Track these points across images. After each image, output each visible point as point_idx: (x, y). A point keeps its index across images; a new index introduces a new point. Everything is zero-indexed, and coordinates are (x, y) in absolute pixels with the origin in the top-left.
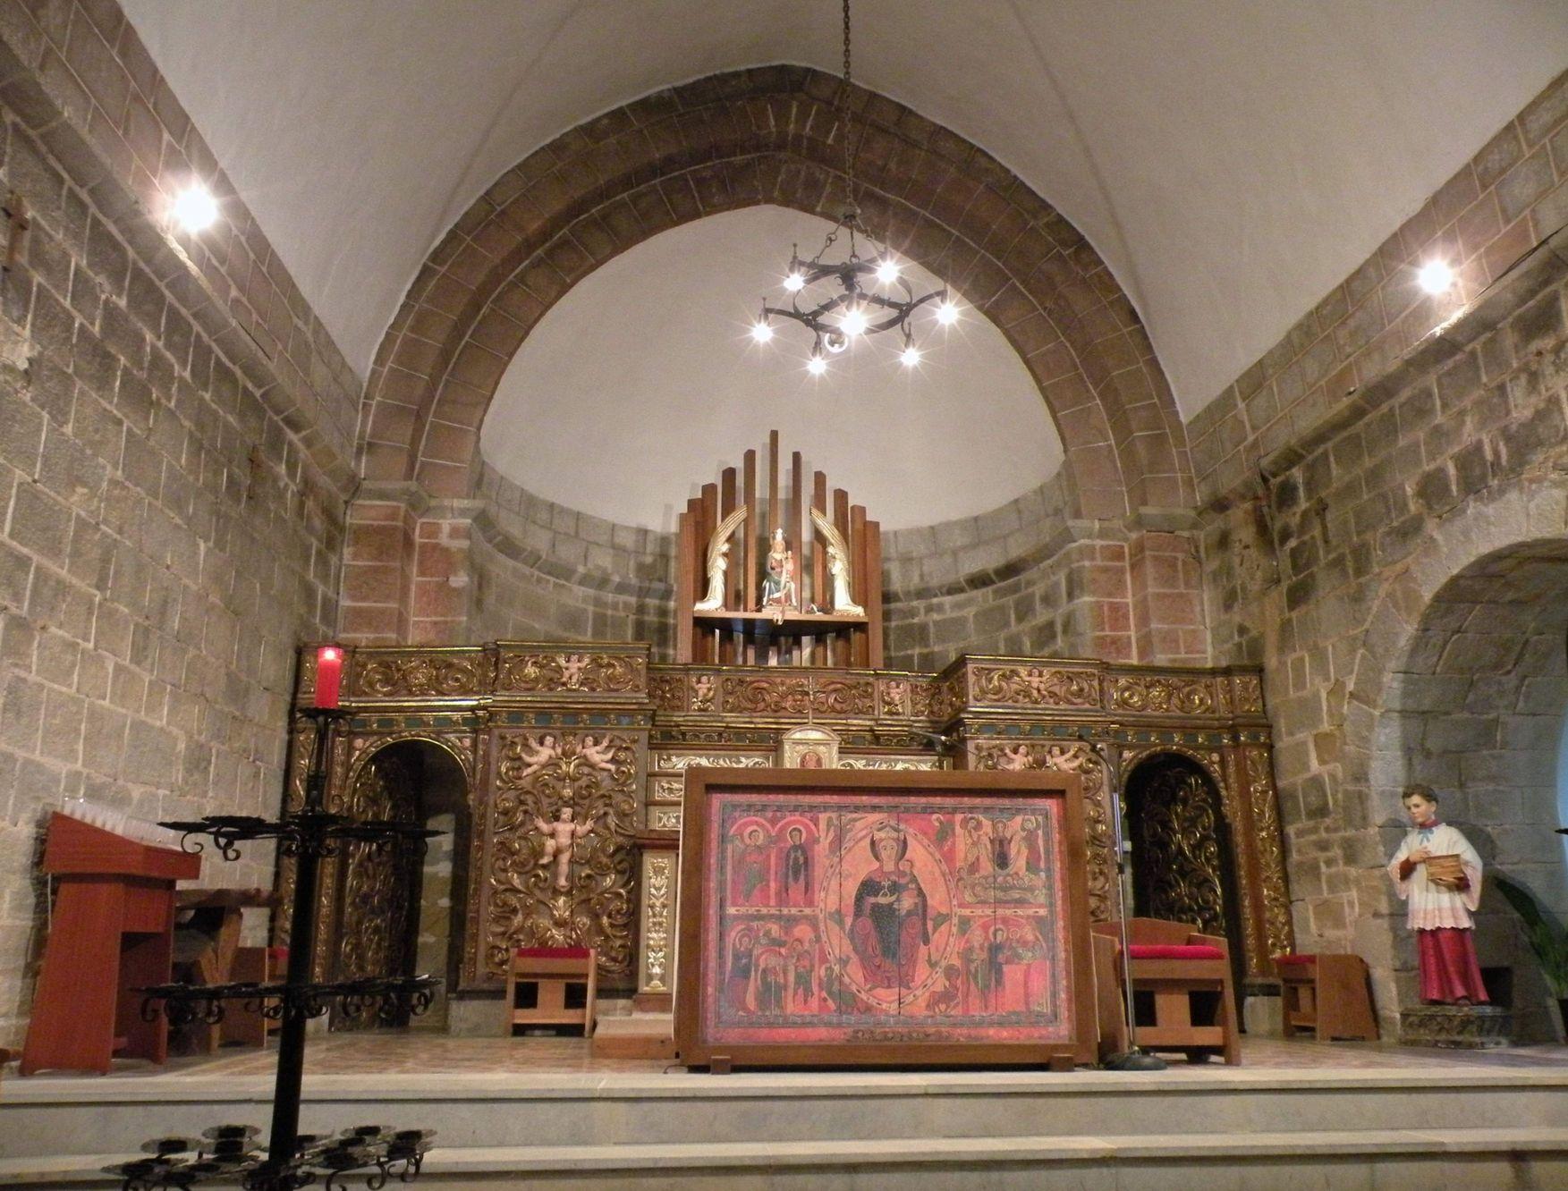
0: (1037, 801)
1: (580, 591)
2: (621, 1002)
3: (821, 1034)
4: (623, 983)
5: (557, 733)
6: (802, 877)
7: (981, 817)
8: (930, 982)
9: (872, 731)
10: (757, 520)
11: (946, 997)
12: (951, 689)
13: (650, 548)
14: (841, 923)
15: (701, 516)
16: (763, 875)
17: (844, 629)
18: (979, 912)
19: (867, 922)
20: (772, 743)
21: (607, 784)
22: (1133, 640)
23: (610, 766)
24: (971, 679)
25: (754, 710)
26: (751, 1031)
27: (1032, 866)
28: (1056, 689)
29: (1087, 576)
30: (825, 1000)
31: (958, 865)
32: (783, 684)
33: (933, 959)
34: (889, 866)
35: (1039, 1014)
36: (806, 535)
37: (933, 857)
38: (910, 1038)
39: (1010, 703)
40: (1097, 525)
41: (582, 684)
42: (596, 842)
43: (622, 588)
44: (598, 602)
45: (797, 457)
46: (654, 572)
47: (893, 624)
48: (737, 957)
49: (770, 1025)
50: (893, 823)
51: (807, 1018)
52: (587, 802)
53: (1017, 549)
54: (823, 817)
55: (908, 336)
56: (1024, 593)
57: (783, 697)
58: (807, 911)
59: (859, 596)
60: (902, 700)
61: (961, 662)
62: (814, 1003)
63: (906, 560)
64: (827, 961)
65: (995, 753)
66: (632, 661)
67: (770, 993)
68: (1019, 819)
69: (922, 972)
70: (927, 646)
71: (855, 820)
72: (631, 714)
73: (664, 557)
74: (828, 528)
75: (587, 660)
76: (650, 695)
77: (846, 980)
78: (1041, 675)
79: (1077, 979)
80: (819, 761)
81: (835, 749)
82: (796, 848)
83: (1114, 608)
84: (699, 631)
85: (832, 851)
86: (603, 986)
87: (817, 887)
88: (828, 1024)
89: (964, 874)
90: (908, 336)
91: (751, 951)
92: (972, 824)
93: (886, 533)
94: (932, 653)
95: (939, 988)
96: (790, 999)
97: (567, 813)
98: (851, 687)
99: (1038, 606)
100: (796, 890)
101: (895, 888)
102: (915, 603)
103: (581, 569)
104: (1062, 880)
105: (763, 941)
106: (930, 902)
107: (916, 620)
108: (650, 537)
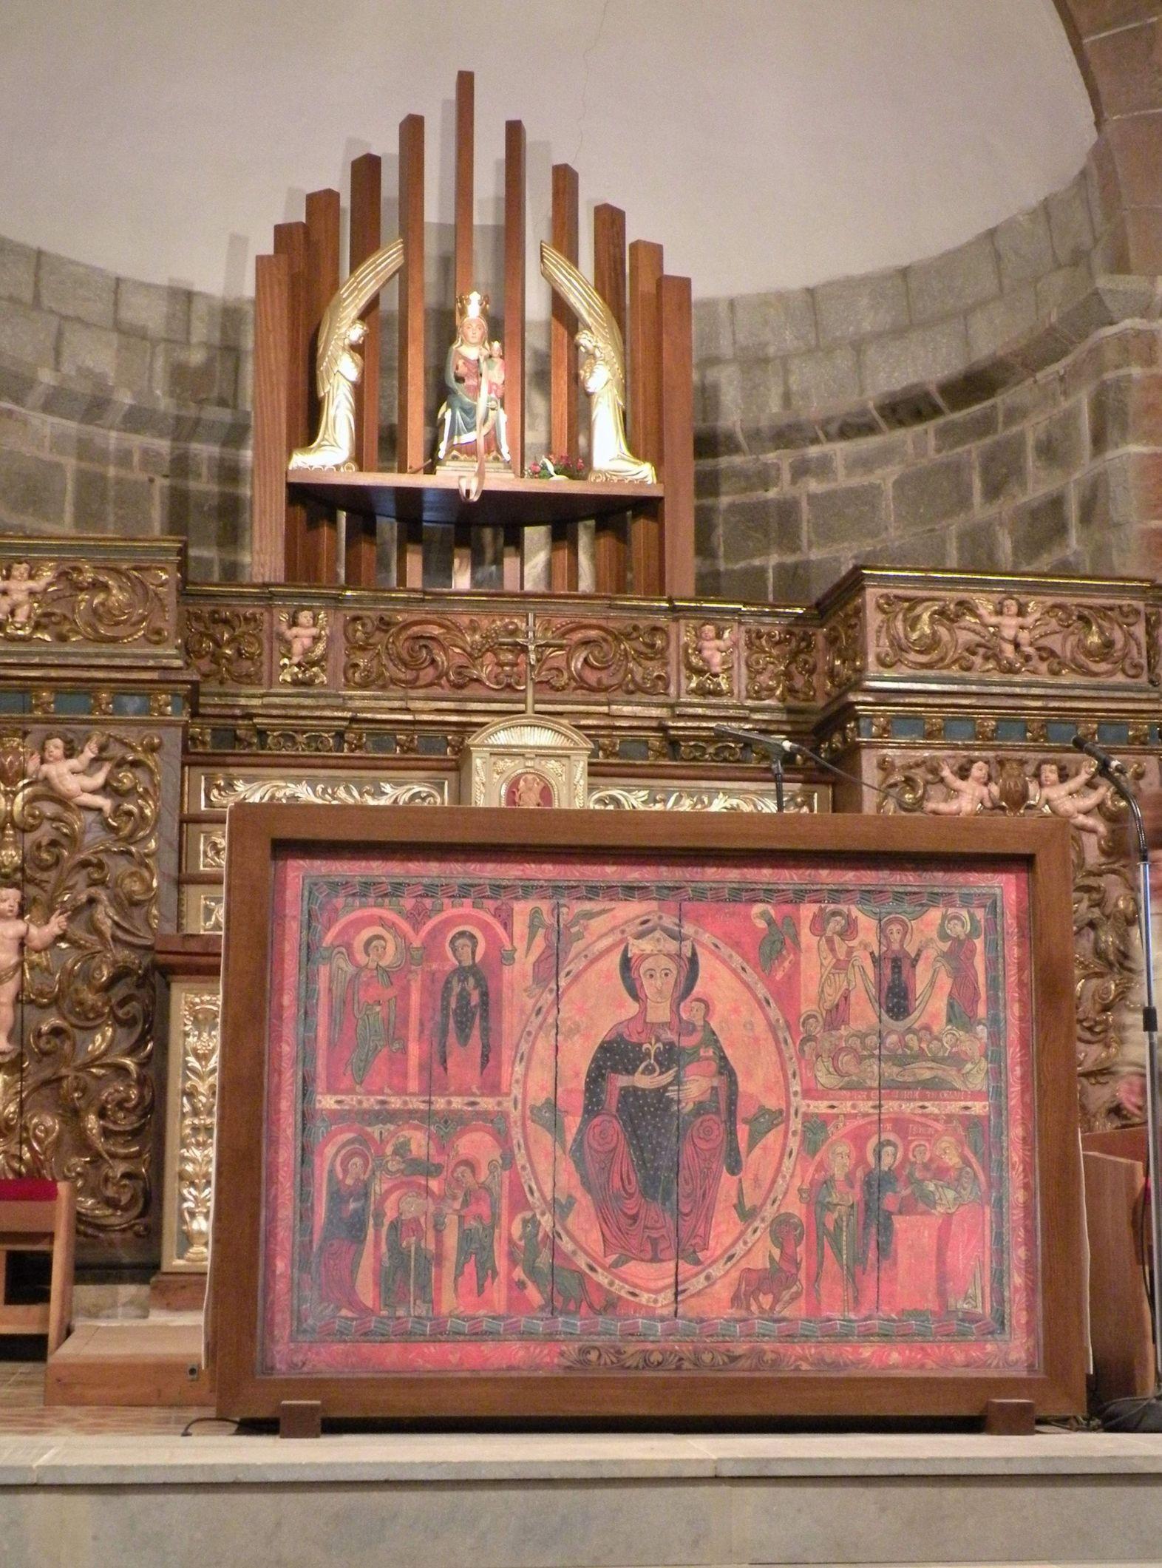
0: (973, 877)
1: (47, 425)
2: (127, 1291)
3: (512, 1355)
4: (127, 1253)
6: (476, 1032)
7: (855, 912)
9: (663, 729)
10: (430, 273)
11: (772, 1280)
12: (832, 641)
13: (200, 331)
14: (556, 1127)
15: (304, 261)
16: (395, 1032)
17: (615, 513)
18: (846, 1107)
19: (611, 1127)
20: (446, 751)
21: (94, 838)
23: (99, 801)
24: (873, 619)
25: (412, 684)
26: (366, 1348)
27: (960, 1014)
28: (1054, 643)
29: (1135, 400)
30: (521, 1285)
31: (805, 1009)
32: (474, 628)
34: (660, 1012)
35: (969, 1318)
36: (536, 306)
37: (756, 994)
38: (697, 1363)
39: (955, 671)
41: (38, 627)
42: (72, 961)
43: (137, 420)
44: (85, 449)
45: (514, 131)
46: (207, 386)
47: (725, 501)
48: (337, 1197)
49: (406, 1336)
50: (669, 921)
51: (482, 1323)
52: (52, 875)
53: (989, 339)
54: (522, 910)
56: (1002, 433)
57: (474, 656)
58: (487, 1103)
59: (643, 437)
60: (726, 664)
61: (853, 583)
62: (498, 1294)
63: (754, 361)
64: (527, 1206)
65: (920, 775)
66: (148, 579)
67: (407, 1271)
68: (935, 915)
69: (724, 1228)
70: (795, 549)
71: (590, 915)
72: (144, 690)
73: (230, 351)
74: (583, 299)
75: (48, 575)
76: (188, 651)
77: (566, 1245)
78: (1021, 612)
79: (1048, 1245)
80: (546, 793)
81: (580, 768)
82: (462, 973)
84: (300, 513)
85: (540, 979)
86: (91, 1256)
87: (506, 1054)
88: (526, 1335)
89: (816, 1028)
91: (366, 1185)
92: (835, 925)
93: (710, 304)
94: (807, 564)
95: (759, 1262)
96: (448, 1282)
98: (618, 637)
99: (1030, 460)
100: (463, 1058)
101: (670, 1057)
102: (771, 457)
103: (46, 377)
104: (1024, 1043)
105: (392, 1166)
106: (743, 1085)
107: (772, 494)
108: (200, 308)
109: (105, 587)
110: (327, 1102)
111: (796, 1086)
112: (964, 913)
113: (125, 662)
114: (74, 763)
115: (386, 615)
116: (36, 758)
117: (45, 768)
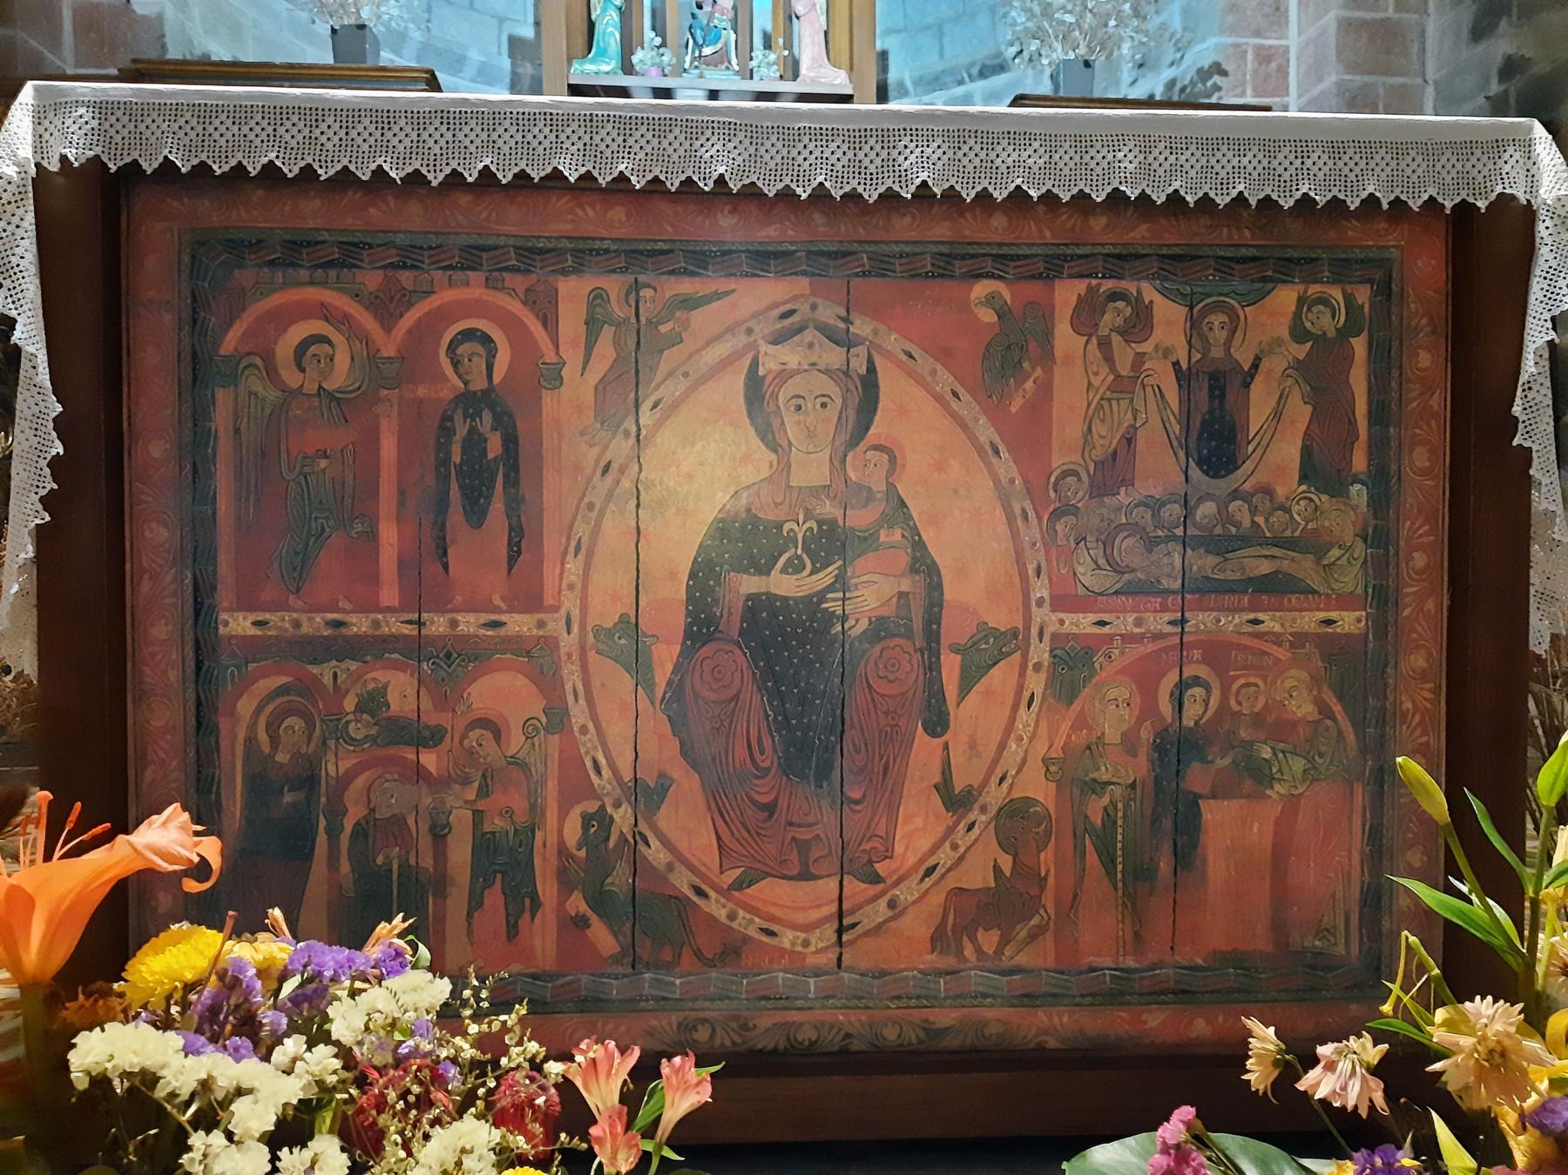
6: (497, 506)
8: (945, 857)
18: (1125, 623)
27: (1320, 471)
30: (582, 923)
33: (959, 784)
34: (812, 469)
58: (519, 624)
68: (1285, 297)
71: (690, 303)
77: (656, 854)
82: (471, 402)
83: (1265, 56)
89: (1077, 492)
92: (1112, 317)
95: (977, 876)
101: (831, 544)
106: (950, 592)
111: (1041, 590)
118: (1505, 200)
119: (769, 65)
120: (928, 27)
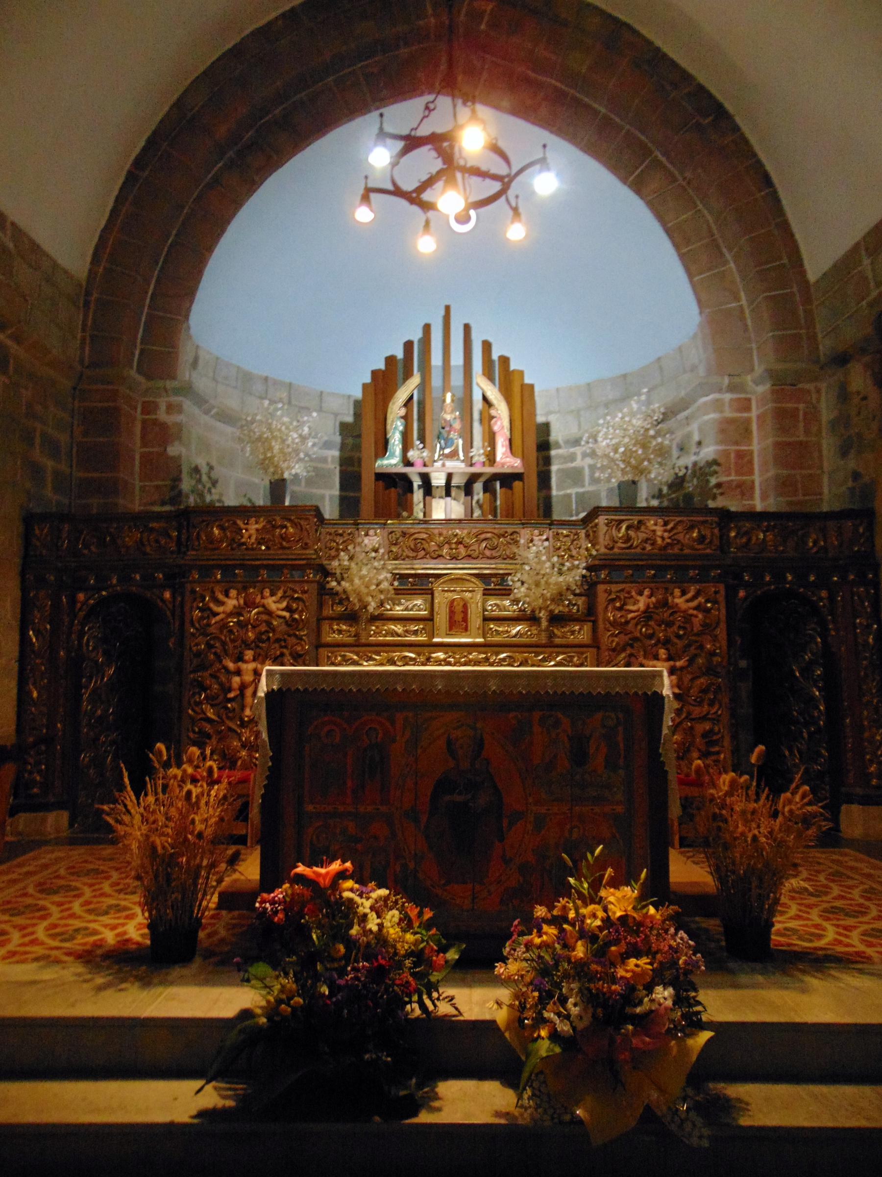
5: (240, 585)
7: (560, 715)
12: (587, 536)
22: (757, 484)
25: (415, 558)
40: (726, 380)
45: (467, 328)
55: (515, 210)
58: (383, 809)
68: (599, 715)
83: (740, 455)
90: (515, 210)
97: (249, 654)
109: (286, 527)
110: (310, 808)
111: (531, 800)
112: (613, 715)
113: (294, 557)
114: (274, 598)
115: (404, 530)
116: (259, 597)
117: (263, 601)
118: (655, 693)
119: (479, 455)
120: (572, 411)
